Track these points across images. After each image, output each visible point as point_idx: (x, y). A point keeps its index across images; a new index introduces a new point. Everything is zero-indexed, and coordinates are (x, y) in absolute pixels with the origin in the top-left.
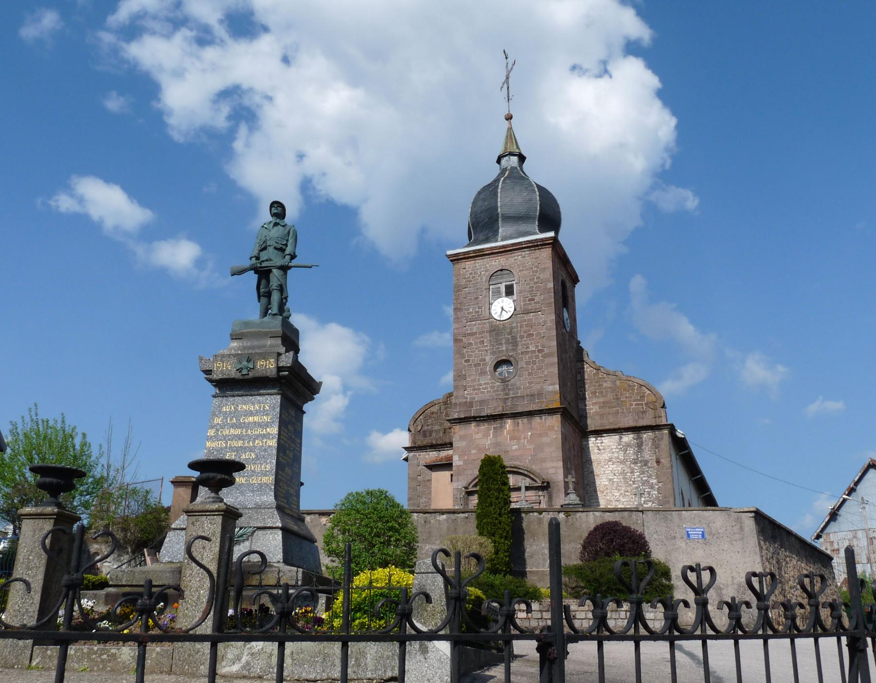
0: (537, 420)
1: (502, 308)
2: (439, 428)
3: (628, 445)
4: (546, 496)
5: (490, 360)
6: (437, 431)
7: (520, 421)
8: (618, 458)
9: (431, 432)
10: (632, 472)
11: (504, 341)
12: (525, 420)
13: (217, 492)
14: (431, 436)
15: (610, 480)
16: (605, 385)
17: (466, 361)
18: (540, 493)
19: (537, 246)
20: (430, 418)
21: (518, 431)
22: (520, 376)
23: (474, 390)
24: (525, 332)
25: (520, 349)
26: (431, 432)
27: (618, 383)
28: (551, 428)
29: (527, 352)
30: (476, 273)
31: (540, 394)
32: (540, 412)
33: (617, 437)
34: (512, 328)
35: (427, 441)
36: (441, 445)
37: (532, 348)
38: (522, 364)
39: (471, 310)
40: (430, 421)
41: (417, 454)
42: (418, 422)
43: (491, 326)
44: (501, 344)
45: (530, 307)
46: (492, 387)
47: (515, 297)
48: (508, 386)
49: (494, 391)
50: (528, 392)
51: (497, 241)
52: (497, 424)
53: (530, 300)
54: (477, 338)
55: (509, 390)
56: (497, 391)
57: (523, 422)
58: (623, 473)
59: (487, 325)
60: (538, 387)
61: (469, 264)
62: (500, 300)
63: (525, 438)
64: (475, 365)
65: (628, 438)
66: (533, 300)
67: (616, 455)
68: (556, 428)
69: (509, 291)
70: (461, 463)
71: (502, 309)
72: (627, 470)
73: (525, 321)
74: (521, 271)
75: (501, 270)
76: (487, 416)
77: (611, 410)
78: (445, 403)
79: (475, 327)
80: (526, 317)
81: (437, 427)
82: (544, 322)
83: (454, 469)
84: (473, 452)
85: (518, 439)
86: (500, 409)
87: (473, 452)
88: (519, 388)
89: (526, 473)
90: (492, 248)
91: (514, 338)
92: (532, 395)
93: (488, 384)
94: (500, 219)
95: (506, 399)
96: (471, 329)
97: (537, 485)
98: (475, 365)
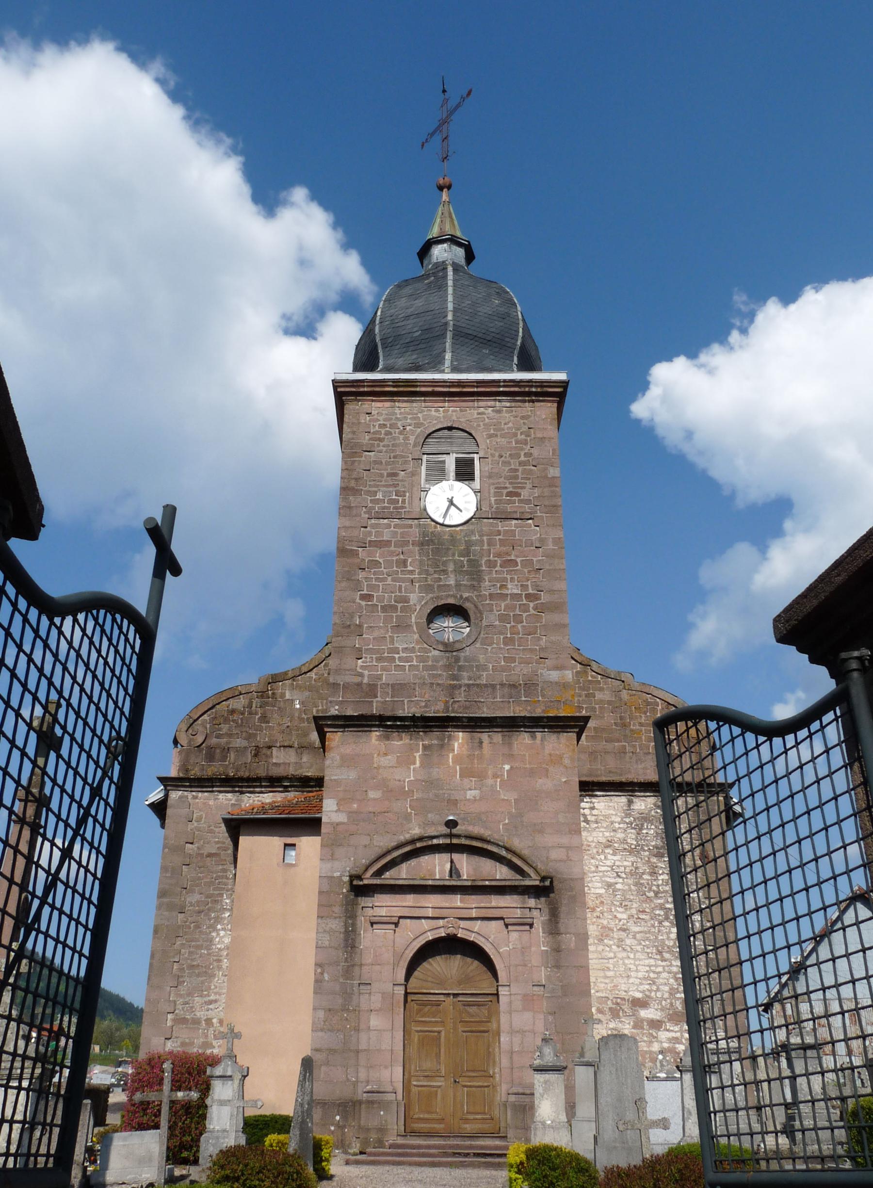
0: (523, 740)
1: (450, 502)
2: (245, 743)
3: (645, 818)
4: (546, 911)
5: (419, 602)
6: (240, 751)
7: (485, 737)
8: (624, 841)
9: (226, 750)
10: (653, 873)
11: (451, 567)
12: (498, 737)
13: (357, 896)
14: (224, 758)
15: (610, 885)
16: (599, 696)
17: (364, 597)
18: (532, 902)
19: (529, 394)
20: (226, 720)
21: (481, 758)
22: (487, 642)
23: (379, 660)
24: (499, 555)
25: (487, 587)
26: (226, 750)
27: (625, 694)
28: (556, 760)
29: (503, 596)
30: (392, 426)
31: (530, 686)
32: (534, 723)
33: (623, 800)
34: (469, 544)
35: (214, 769)
36: (241, 779)
37: (513, 588)
38: (491, 618)
39: (379, 496)
40: (225, 728)
41: (190, 795)
42: (198, 726)
43: (424, 534)
44: (445, 572)
45: (509, 508)
46: (421, 659)
47: (477, 484)
48: (457, 659)
49: (426, 668)
50: (504, 677)
51: (443, 372)
52: (432, 738)
53: (509, 494)
54: (392, 554)
55: (460, 668)
56: (433, 668)
57: (490, 740)
58: (635, 873)
59: (415, 531)
60: (527, 670)
61: (379, 408)
62: (444, 484)
63: (495, 776)
64: (384, 609)
65: (646, 803)
66: (519, 495)
67: (620, 835)
68: (567, 761)
69: (465, 472)
70: (342, 818)
71: (451, 502)
72: (643, 868)
73: (499, 533)
74: (490, 436)
75: (450, 428)
76: (413, 718)
77: (609, 746)
78: (262, 694)
79: (388, 530)
80: (501, 526)
81: (239, 743)
82: (542, 540)
83: (324, 830)
84: (372, 794)
85: (481, 776)
86: (440, 706)
87: (372, 794)
88: (482, 668)
89: (504, 853)
90: (434, 383)
91: (474, 563)
92: (513, 686)
93: (413, 650)
94: (449, 335)
95: (454, 687)
96: (378, 534)
97: (528, 882)
98: (384, 609)
